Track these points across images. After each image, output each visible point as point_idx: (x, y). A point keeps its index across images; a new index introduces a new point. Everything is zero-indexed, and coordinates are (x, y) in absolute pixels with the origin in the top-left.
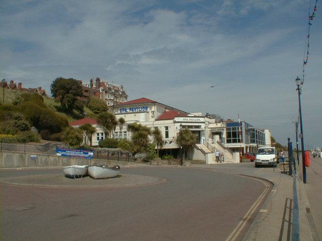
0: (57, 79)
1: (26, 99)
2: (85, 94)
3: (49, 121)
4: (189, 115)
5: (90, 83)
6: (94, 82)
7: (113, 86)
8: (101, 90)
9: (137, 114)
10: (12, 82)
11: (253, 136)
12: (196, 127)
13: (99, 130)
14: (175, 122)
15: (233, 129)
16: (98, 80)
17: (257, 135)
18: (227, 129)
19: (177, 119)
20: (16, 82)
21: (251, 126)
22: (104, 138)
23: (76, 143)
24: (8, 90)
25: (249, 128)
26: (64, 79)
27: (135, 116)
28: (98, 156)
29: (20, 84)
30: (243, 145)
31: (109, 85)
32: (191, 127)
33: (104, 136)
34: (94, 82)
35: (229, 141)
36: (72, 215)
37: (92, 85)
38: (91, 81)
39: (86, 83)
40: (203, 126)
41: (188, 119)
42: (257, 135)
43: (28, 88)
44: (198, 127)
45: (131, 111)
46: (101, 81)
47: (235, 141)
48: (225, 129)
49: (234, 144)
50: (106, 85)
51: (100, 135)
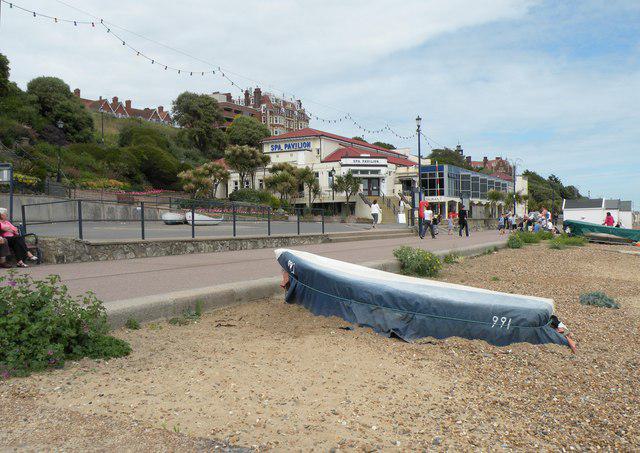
0: (34, 81)
1: (299, 119)
2: (226, 115)
9: (294, 153)
10: (115, 99)
12: (373, 172)
13: (235, 176)
14: (343, 165)
19: (344, 161)
20: (122, 100)
23: (200, 200)
26: (195, 96)
27: (291, 155)
29: (128, 103)
33: (239, 185)
36: (418, 131)
37: (247, 101)
38: (247, 94)
40: (383, 170)
43: (142, 109)
44: (377, 172)
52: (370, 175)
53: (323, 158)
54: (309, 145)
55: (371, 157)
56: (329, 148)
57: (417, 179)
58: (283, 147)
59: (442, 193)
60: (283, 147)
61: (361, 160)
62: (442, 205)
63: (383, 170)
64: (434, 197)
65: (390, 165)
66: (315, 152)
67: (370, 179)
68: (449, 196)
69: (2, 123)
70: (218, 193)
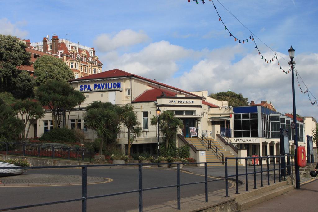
3: (62, 133)
4: (178, 96)
5: (42, 43)
6: (49, 42)
7: (79, 49)
8: (59, 55)
9: (104, 93)
11: (275, 126)
15: (245, 116)
16: (55, 39)
17: (268, 120)
18: (235, 117)
19: (160, 101)
21: (275, 112)
22: (49, 128)
24: (60, 96)
25: (271, 115)
27: (102, 95)
28: (40, 153)
30: (259, 140)
31: (72, 47)
32: (181, 112)
34: (49, 42)
35: (237, 135)
37: (45, 47)
38: (45, 41)
39: (36, 45)
40: (198, 111)
41: (177, 102)
42: (268, 120)
44: (192, 112)
45: (96, 89)
46: (60, 41)
47: (247, 135)
48: (233, 116)
49: (245, 139)
50: (68, 47)
51: (49, 123)
52: (185, 116)
53: (133, 99)
54: (119, 85)
55: (186, 98)
56: (140, 89)
57: (232, 120)
58: (92, 87)
59: (255, 134)
60: (92, 87)
61: (177, 100)
62: (256, 146)
63: (198, 111)
64: (249, 138)
65: (204, 106)
66: (125, 93)
67: (185, 120)
68: (266, 135)
69: (317, 169)
70: (29, 132)
